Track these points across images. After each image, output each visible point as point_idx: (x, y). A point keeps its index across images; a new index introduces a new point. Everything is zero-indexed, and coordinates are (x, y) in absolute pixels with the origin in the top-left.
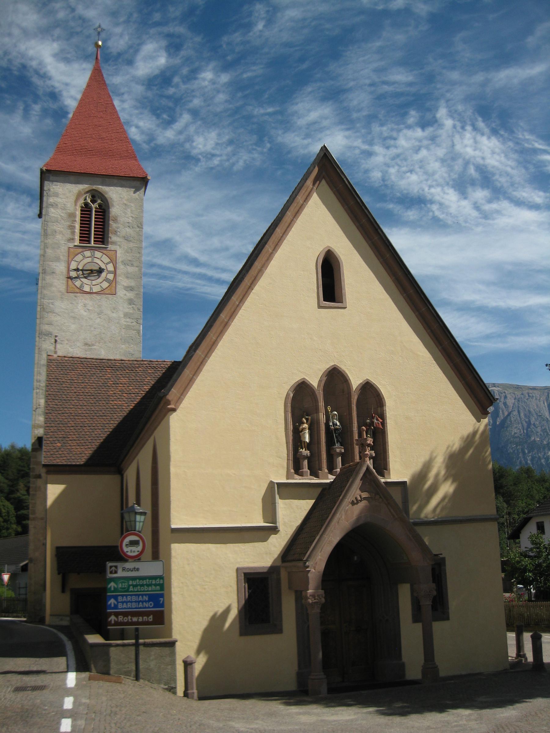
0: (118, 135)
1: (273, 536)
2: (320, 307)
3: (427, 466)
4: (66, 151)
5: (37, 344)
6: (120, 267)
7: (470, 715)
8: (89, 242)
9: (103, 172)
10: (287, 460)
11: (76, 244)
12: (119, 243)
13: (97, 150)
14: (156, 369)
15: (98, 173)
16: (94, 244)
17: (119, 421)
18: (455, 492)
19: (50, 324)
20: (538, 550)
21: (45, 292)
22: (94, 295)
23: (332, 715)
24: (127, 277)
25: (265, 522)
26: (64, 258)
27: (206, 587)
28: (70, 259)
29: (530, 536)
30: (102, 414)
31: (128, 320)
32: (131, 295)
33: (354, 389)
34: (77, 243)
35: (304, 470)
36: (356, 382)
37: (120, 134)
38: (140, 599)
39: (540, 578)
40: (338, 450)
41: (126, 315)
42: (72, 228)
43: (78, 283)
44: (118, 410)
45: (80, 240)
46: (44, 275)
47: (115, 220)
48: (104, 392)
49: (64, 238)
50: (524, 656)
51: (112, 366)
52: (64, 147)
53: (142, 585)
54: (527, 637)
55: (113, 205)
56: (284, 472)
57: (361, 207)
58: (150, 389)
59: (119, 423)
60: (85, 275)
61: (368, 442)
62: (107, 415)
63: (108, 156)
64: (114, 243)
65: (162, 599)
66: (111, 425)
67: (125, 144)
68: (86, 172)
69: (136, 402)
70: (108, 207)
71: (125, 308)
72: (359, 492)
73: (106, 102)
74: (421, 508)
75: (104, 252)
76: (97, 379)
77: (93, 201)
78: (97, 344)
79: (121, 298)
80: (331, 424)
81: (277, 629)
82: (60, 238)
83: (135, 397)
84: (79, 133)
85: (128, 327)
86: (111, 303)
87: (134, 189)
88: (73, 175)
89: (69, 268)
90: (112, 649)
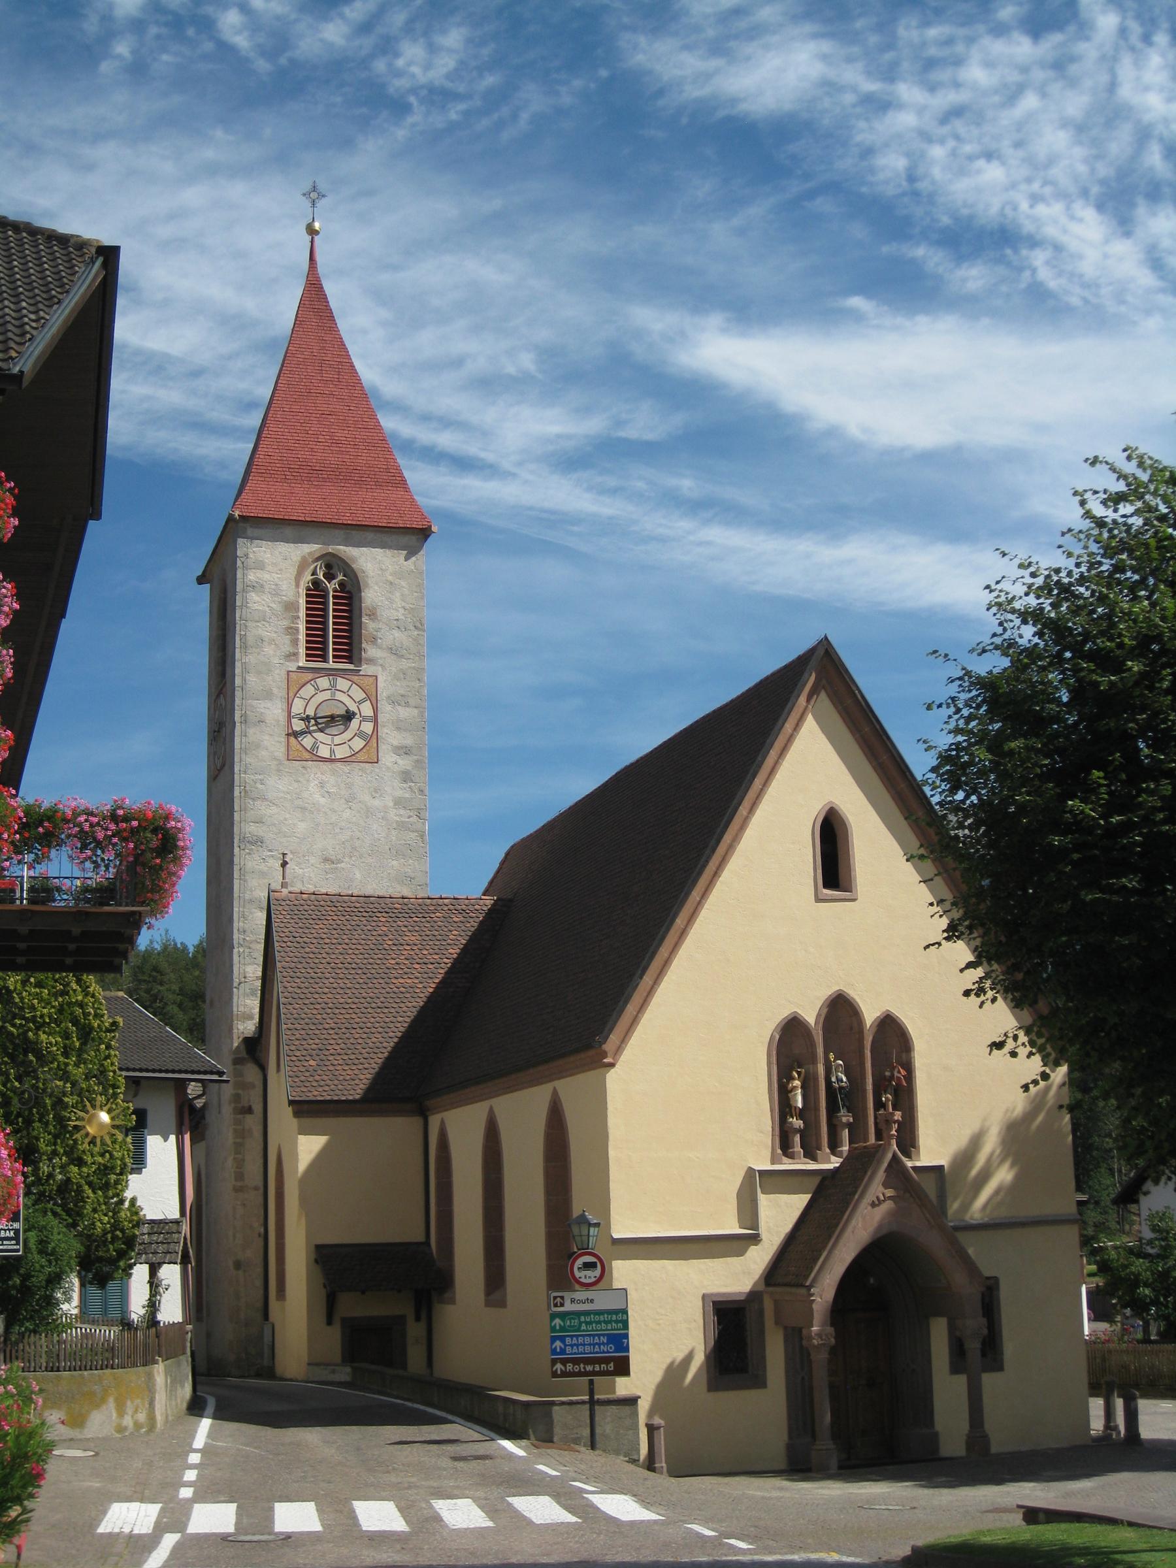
0: (367, 434)
1: (752, 1247)
2: (818, 899)
3: (976, 1142)
4: (272, 472)
5: (236, 860)
6: (385, 708)
7: (1034, 1486)
8: (324, 658)
9: (347, 518)
10: (772, 1135)
11: (301, 664)
12: (380, 662)
13: (329, 469)
14: (467, 915)
15: (339, 522)
16: (333, 662)
17: (413, 1017)
18: (1017, 1178)
19: (259, 821)
20: (1163, 1243)
21: (249, 759)
22: (339, 764)
23: (859, 1488)
24: (398, 729)
25: (741, 1227)
26: (280, 692)
27: (661, 1322)
28: (291, 695)
29: (1148, 1216)
30: (380, 1004)
31: (402, 812)
32: (405, 763)
33: (868, 1026)
34: (302, 662)
35: (795, 1150)
36: (870, 1015)
37: (370, 430)
38: (595, 1341)
39: (1166, 1297)
40: (844, 1120)
41: (398, 802)
42: (292, 631)
43: (307, 741)
44: (408, 995)
45: (307, 655)
46: (243, 727)
47: (373, 615)
48: (379, 962)
49: (278, 653)
50: (1116, 1428)
51: (387, 910)
52: (267, 464)
53: (599, 1322)
54: (1119, 1403)
55: (367, 585)
56: (767, 1153)
57: (881, 736)
58: (459, 954)
59: (413, 1021)
60: (320, 726)
61: (896, 1118)
62: (389, 1005)
63: (353, 482)
64: (371, 661)
65: (626, 1341)
66: (399, 1025)
67: (382, 453)
68: (315, 520)
69: (437, 981)
70: (359, 590)
71: (395, 789)
72: (881, 1188)
73: (338, 360)
74: (966, 1206)
75: (355, 678)
76: (363, 937)
77: (330, 577)
78: (347, 859)
79: (388, 768)
80: (834, 1079)
81: (758, 1381)
82: (271, 652)
83: (435, 971)
84: (291, 431)
85: (402, 826)
86: (369, 778)
87: (405, 552)
88: (289, 525)
89: (289, 712)
90: (556, 1408)
